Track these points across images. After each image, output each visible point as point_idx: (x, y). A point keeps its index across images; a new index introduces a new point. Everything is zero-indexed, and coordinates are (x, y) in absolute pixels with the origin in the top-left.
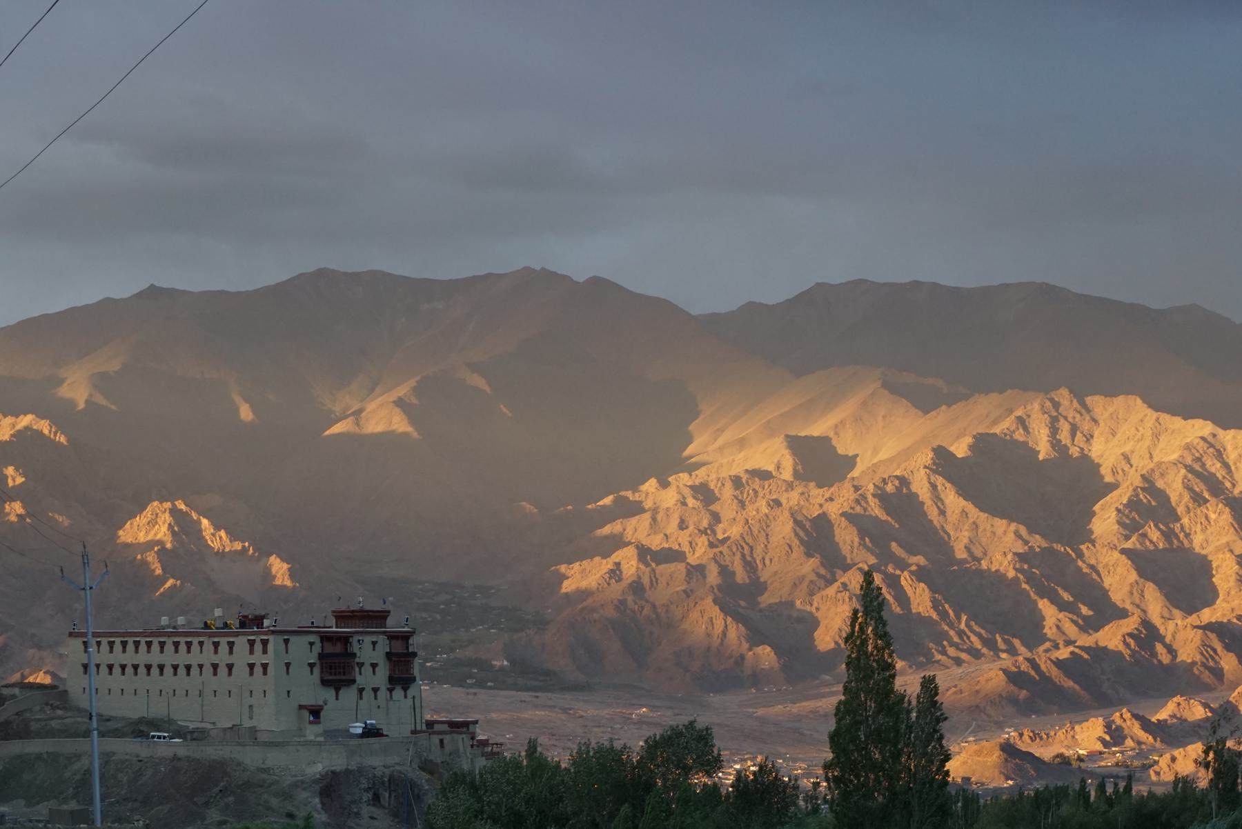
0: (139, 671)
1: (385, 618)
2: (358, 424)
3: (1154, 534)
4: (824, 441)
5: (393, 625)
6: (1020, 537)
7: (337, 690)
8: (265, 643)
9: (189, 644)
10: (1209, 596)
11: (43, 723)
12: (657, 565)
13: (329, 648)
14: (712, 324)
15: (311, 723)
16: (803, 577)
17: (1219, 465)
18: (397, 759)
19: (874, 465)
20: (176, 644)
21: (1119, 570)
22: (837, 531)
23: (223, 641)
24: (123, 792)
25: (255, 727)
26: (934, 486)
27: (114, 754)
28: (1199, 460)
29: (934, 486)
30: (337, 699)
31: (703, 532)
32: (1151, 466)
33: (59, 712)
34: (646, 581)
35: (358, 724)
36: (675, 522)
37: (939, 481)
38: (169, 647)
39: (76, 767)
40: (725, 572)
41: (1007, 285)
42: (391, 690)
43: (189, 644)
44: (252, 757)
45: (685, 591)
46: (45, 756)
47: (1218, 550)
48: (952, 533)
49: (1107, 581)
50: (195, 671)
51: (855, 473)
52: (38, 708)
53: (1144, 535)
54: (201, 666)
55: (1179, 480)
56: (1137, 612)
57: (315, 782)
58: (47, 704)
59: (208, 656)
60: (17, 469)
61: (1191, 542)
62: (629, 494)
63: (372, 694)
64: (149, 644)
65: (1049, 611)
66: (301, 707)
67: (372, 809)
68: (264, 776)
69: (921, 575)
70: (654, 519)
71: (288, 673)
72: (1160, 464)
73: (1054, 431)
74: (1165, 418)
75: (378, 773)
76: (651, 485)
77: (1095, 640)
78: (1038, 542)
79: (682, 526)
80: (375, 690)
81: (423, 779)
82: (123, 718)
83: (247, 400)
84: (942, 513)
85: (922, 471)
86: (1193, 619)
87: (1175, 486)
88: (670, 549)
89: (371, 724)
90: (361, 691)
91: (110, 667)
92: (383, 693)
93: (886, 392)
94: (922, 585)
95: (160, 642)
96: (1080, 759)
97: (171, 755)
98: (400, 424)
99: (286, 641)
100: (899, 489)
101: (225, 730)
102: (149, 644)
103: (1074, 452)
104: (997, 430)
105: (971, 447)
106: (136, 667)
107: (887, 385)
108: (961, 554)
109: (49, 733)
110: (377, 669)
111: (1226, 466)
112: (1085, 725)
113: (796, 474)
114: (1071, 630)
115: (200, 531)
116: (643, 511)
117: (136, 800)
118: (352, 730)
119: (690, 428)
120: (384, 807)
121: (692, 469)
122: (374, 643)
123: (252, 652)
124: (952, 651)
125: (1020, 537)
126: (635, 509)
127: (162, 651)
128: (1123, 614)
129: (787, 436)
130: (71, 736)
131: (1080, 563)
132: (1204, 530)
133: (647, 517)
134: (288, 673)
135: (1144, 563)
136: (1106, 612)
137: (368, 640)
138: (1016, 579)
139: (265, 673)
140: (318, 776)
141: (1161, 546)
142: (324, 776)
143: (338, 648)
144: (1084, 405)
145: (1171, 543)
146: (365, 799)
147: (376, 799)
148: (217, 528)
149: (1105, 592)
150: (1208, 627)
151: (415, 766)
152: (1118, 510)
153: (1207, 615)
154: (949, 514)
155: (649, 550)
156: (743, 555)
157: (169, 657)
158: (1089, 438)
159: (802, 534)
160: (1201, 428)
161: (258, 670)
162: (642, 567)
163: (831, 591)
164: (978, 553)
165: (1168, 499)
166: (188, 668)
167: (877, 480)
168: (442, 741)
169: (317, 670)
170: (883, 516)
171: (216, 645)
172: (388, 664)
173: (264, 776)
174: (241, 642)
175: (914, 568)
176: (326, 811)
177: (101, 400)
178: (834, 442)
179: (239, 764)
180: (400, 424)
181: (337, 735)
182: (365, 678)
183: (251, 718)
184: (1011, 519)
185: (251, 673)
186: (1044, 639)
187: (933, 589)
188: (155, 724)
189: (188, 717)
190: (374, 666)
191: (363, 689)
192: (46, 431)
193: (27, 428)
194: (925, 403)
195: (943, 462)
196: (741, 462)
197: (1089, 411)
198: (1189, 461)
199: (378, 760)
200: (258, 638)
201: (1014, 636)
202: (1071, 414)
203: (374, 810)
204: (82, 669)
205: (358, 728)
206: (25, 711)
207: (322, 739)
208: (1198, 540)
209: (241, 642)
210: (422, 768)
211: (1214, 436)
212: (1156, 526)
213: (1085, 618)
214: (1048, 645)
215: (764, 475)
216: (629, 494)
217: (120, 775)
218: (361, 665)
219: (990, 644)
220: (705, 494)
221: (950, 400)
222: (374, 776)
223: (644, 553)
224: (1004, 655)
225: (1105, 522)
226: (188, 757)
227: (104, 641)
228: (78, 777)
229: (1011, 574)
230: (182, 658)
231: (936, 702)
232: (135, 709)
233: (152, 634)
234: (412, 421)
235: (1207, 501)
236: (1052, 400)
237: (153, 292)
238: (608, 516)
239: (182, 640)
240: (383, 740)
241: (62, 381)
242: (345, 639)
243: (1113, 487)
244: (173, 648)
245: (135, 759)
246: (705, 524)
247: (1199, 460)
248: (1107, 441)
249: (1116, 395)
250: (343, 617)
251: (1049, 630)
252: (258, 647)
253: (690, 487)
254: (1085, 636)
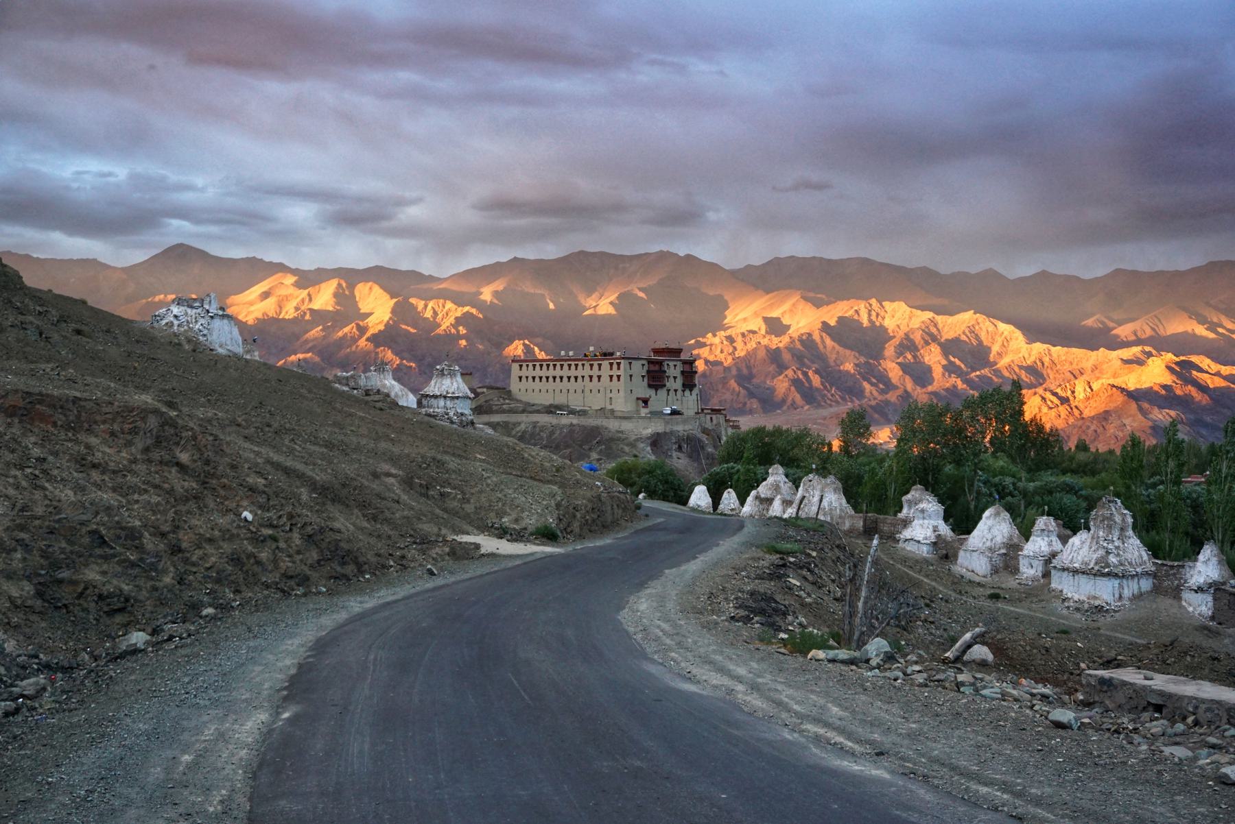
1: (680, 353)
3: (909, 357)
4: (778, 319)
5: (683, 357)
6: (856, 357)
7: (656, 390)
8: (619, 364)
10: (930, 380)
13: (653, 368)
14: (734, 274)
15: (643, 407)
18: (691, 428)
23: (595, 363)
26: (822, 337)
28: (927, 327)
29: (822, 337)
31: (730, 354)
32: (908, 329)
33: (507, 401)
34: (708, 373)
36: (719, 350)
37: (824, 334)
40: (739, 370)
42: (683, 391)
44: (613, 425)
50: (580, 379)
51: (790, 331)
53: (905, 357)
54: (583, 377)
57: (648, 438)
62: (701, 339)
65: (866, 385)
66: (638, 399)
68: (621, 435)
69: (817, 372)
72: (912, 329)
73: (870, 315)
75: (681, 434)
76: (710, 335)
78: (862, 360)
79: (722, 352)
80: (676, 391)
84: (825, 347)
86: (924, 390)
87: (917, 337)
90: (668, 391)
92: (680, 393)
96: (881, 444)
98: (611, 310)
99: (630, 363)
101: (597, 410)
103: (878, 324)
104: (847, 315)
105: (837, 322)
106: (547, 378)
108: (832, 364)
109: (504, 412)
111: (938, 330)
113: (767, 332)
116: (707, 346)
122: (675, 366)
123: (611, 369)
124: (829, 402)
125: (856, 357)
126: (704, 345)
127: (555, 369)
128: (896, 388)
130: (514, 413)
132: (929, 355)
135: (905, 368)
136: (888, 385)
137: (671, 364)
138: (854, 374)
139: (619, 380)
141: (912, 361)
142: (653, 435)
143: (657, 368)
144: (881, 305)
146: (674, 448)
147: (680, 448)
148: (541, 350)
153: (930, 388)
155: (709, 361)
158: (883, 318)
160: (930, 315)
161: (615, 378)
163: (781, 377)
164: (838, 362)
167: (799, 334)
168: (711, 418)
169: (646, 379)
171: (592, 366)
173: (621, 435)
176: (654, 454)
179: (606, 428)
180: (611, 310)
182: (670, 384)
183: (611, 404)
184: (852, 350)
185: (611, 380)
186: (865, 397)
187: (821, 377)
190: (675, 378)
193: (467, 312)
194: (818, 304)
195: (825, 327)
196: (744, 328)
197: (883, 307)
198: (923, 328)
199: (680, 428)
200: (615, 362)
202: (876, 309)
208: (926, 359)
209: (605, 364)
210: (703, 433)
213: (882, 389)
214: (866, 400)
215: (754, 332)
216: (701, 339)
217: (542, 434)
219: (843, 398)
220: (731, 339)
224: (849, 404)
225: (890, 350)
227: (531, 364)
229: (852, 371)
230: (573, 373)
231: (1021, 394)
232: (546, 400)
233: (556, 360)
234: (616, 310)
237: (515, 259)
239: (573, 363)
240: (683, 417)
241: (481, 293)
242: (660, 363)
243: (894, 337)
246: (731, 351)
247: (927, 327)
249: (894, 301)
250: (657, 351)
251: (867, 393)
252: (615, 366)
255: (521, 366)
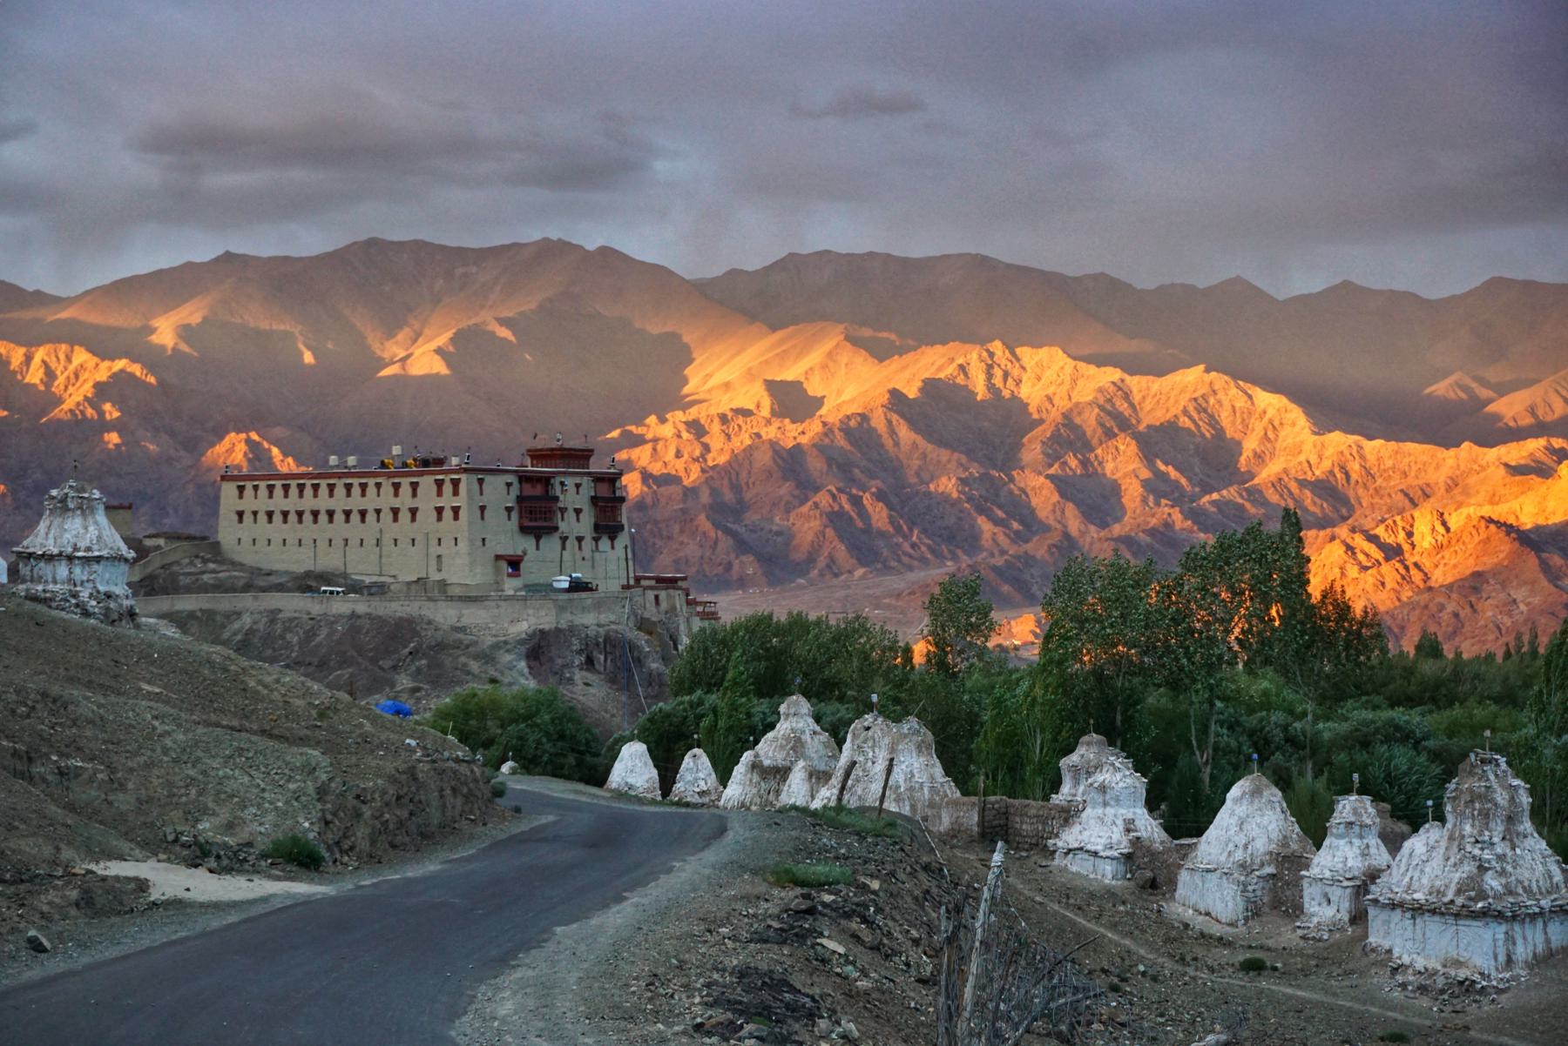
0: (304, 517)
1: (588, 458)
2: (404, 369)
4: (796, 386)
5: (596, 466)
7: (538, 539)
8: (456, 483)
9: (364, 487)
11: (193, 578)
12: (658, 487)
13: (529, 490)
15: (510, 575)
16: (781, 498)
17: (1126, 405)
18: (613, 618)
19: (839, 405)
20: (348, 487)
21: (1044, 492)
22: (809, 459)
23: (405, 483)
24: (294, 655)
25: (444, 580)
26: (890, 422)
27: (280, 611)
28: (1110, 401)
29: (890, 422)
30: (538, 548)
31: (696, 460)
32: (1069, 406)
33: (212, 566)
34: (649, 500)
35: (562, 578)
36: (672, 452)
37: (895, 417)
38: (340, 491)
39: (236, 626)
40: (714, 492)
41: (948, 256)
42: (596, 540)
43: (364, 487)
44: (445, 615)
45: (681, 509)
46: (199, 614)
47: (1125, 475)
48: (369, 611)
49: (1034, 502)
50: (371, 517)
51: (823, 411)
52: (187, 561)
53: (1065, 463)
54: (378, 512)
55: (1093, 417)
56: (1059, 526)
57: (521, 642)
58: (197, 557)
59: (387, 500)
60: (113, 405)
61: (1103, 469)
62: (633, 428)
63: (576, 543)
64: (316, 487)
65: (985, 526)
66: (498, 557)
67: (584, 673)
68: (461, 636)
69: (880, 496)
70: (655, 449)
71: (483, 518)
72: (1077, 404)
74: (1081, 365)
77: (1502, 471)
79: (678, 455)
80: (580, 539)
81: (642, 639)
82: (286, 572)
83: (309, 348)
84: (897, 444)
85: (880, 410)
88: (669, 474)
89: (577, 578)
90: (564, 539)
91: (270, 515)
92: (588, 544)
93: (848, 344)
94: (881, 504)
95: (329, 485)
96: (1016, 648)
97: (348, 612)
98: (439, 367)
99: (481, 481)
100: (860, 424)
101: (409, 584)
102: (316, 487)
103: (1006, 394)
104: (942, 375)
105: (921, 390)
107: (847, 338)
109: (204, 589)
110: (581, 516)
111: (1132, 405)
112: (1019, 620)
113: (774, 413)
114: (1003, 540)
115: (271, 458)
117: (310, 664)
118: (556, 585)
119: (686, 372)
120: (599, 673)
121: (685, 407)
122: (578, 486)
123: (440, 494)
124: (905, 559)
126: (639, 441)
128: (1048, 528)
129: (765, 381)
130: (226, 591)
131: (1012, 486)
132: (1115, 459)
133: (649, 447)
134: (483, 518)
135: (1064, 486)
137: (570, 482)
139: (456, 517)
140: (524, 636)
142: (531, 636)
144: (1013, 354)
145: (1087, 470)
147: (590, 663)
148: (286, 455)
149: (1033, 511)
150: (1119, 539)
151: (631, 625)
152: (1043, 443)
153: (1117, 530)
154: (902, 443)
155: (651, 476)
156: (730, 479)
157: (339, 502)
158: (1018, 382)
159: (779, 461)
161: (448, 514)
162: (646, 489)
163: (805, 509)
164: (926, 476)
165: (1084, 433)
166: (363, 513)
168: (657, 597)
169: (515, 515)
170: (848, 447)
171: (396, 486)
172: (593, 510)
173: (461, 636)
174: (427, 483)
175: (874, 490)
177: (184, 347)
178: (805, 386)
179: (429, 622)
181: (542, 590)
182: (567, 525)
183: (440, 570)
185: (439, 519)
188: (326, 578)
189: (363, 567)
190: (578, 512)
191: (566, 538)
192: (138, 374)
193: (122, 371)
194: (880, 353)
197: (1018, 360)
198: (1101, 401)
199: (590, 620)
200: (447, 478)
201: (958, 547)
202: (1003, 362)
203: (589, 676)
204: (236, 518)
205: (563, 582)
206: (171, 564)
207: (523, 593)
208: (1109, 467)
211: (1123, 381)
212: (1075, 455)
213: (1017, 533)
215: (746, 413)
216: (633, 428)
218: (563, 510)
220: (696, 428)
221: (902, 351)
222: (587, 636)
223: (646, 477)
224: (949, 563)
225: (1032, 451)
226: (369, 615)
227: (263, 485)
228: (239, 637)
229: (955, 495)
230: (356, 502)
232: (299, 561)
233: (319, 476)
234: (449, 365)
235: (1116, 435)
236: (988, 351)
238: (618, 445)
239: (356, 482)
240: (595, 595)
242: (546, 480)
243: (1041, 421)
244: (344, 491)
245: (306, 617)
246: (697, 453)
247: (1110, 401)
248: (1033, 385)
250: (538, 456)
253: (685, 423)
254: (1015, 547)
255: (241, 489)
